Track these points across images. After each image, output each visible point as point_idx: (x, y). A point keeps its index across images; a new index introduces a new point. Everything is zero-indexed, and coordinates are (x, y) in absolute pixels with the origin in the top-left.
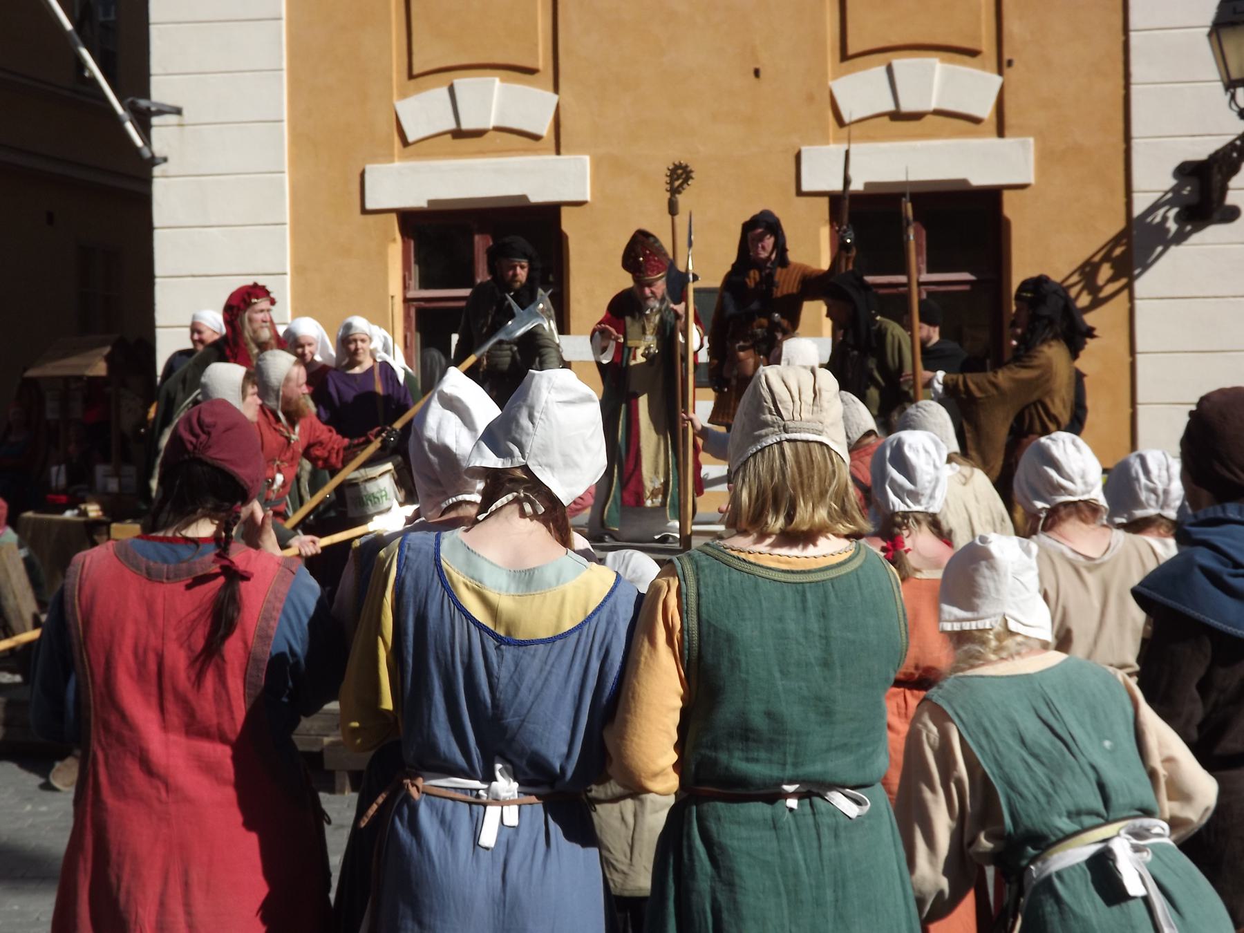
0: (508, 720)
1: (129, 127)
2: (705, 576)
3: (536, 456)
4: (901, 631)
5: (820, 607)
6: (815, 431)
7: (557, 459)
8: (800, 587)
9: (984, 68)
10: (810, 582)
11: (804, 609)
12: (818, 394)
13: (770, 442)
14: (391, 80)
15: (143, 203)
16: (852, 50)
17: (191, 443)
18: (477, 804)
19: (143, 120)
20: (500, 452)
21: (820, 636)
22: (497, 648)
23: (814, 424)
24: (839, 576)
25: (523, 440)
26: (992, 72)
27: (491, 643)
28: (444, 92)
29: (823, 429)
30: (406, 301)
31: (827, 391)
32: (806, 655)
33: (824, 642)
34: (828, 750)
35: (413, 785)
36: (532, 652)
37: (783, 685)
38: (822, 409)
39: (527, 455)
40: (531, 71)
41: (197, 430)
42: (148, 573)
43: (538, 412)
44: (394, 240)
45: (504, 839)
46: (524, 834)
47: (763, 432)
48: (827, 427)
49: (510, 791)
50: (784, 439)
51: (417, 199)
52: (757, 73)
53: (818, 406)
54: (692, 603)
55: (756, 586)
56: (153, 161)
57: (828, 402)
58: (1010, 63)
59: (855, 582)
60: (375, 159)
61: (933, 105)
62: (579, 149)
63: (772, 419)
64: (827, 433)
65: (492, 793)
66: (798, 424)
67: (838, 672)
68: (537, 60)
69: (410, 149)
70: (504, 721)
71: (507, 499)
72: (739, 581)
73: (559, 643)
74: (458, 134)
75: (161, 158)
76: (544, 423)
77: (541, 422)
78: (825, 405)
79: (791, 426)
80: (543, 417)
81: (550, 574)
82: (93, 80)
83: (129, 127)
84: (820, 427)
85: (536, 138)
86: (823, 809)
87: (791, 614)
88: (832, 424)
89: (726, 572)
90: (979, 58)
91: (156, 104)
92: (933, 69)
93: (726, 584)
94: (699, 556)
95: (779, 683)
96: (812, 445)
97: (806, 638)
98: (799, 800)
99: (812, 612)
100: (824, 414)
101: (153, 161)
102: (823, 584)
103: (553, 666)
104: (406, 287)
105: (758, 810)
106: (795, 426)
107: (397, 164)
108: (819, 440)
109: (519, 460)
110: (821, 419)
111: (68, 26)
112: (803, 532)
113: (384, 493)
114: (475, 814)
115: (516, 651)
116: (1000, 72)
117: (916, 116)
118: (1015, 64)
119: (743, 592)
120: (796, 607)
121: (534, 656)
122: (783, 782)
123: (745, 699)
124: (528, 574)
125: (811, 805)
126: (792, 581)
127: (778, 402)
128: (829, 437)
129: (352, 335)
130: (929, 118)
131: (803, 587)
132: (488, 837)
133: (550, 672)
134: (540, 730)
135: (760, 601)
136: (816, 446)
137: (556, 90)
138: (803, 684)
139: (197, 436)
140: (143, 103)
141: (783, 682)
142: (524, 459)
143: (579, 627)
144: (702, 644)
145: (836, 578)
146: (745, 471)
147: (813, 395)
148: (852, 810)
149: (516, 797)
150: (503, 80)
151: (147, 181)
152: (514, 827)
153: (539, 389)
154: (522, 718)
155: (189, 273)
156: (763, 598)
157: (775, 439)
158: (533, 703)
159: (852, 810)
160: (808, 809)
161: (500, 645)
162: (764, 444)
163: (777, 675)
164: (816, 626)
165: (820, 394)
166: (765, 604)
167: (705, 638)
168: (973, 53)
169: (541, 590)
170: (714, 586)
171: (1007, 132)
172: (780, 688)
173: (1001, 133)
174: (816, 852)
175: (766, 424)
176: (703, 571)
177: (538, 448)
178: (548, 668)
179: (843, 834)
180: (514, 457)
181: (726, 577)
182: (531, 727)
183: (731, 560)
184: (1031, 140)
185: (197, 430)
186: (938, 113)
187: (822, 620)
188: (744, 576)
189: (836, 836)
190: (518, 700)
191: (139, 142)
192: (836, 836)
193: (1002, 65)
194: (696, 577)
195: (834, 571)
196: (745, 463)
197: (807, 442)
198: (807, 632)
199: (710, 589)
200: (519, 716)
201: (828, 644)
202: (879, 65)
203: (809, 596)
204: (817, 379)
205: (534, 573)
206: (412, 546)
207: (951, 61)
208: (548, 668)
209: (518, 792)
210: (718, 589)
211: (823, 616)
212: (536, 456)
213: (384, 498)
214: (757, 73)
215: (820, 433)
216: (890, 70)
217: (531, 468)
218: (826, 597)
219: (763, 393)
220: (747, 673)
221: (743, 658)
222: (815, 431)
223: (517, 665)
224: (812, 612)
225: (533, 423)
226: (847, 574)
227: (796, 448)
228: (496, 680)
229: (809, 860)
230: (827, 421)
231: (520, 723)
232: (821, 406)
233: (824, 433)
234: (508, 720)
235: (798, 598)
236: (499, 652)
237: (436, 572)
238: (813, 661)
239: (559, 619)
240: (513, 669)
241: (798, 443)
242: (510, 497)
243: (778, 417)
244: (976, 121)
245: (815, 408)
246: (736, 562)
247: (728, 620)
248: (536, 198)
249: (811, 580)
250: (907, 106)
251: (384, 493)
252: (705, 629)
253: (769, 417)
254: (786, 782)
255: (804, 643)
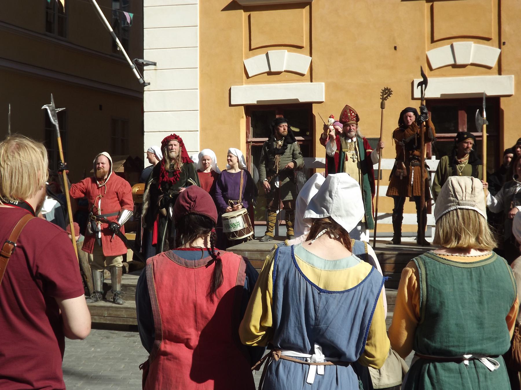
0: (321, 326)
1: (135, 70)
2: (429, 266)
3: (334, 212)
4: (514, 290)
5: (478, 278)
6: (472, 205)
7: (343, 213)
8: (469, 270)
9: (492, 46)
10: (474, 267)
11: (471, 279)
12: (474, 189)
13: (452, 209)
14: (242, 51)
15: (140, 101)
16: (435, 39)
17: (188, 207)
18: (305, 363)
19: (141, 68)
20: (317, 212)
21: (478, 290)
22: (319, 293)
23: (471, 202)
24: (486, 265)
25: (328, 206)
26: (496, 47)
27: (316, 292)
28: (264, 56)
29: (475, 205)
30: (247, 142)
31: (478, 188)
32: (472, 299)
33: (480, 293)
34: (482, 340)
35: (276, 354)
36: (334, 297)
37: (463, 312)
38: (475, 196)
39: (330, 212)
40: (301, 47)
41: (189, 201)
42: (186, 265)
43: (334, 193)
44: (243, 117)
45: (317, 381)
46: (326, 378)
47: (449, 204)
48: (477, 203)
49: (321, 359)
50: (458, 208)
51: (252, 100)
52: (395, 48)
53: (473, 194)
54: (424, 277)
55: (451, 270)
56: (144, 85)
57: (478, 193)
58: (504, 43)
59: (493, 267)
60: (235, 83)
61: (471, 62)
62: (320, 80)
63: (453, 199)
64: (477, 206)
65: (313, 359)
66: (464, 202)
67: (486, 306)
68: (303, 43)
69: (432, 72)
70: (320, 326)
71: (323, 232)
72: (444, 268)
73: (346, 293)
74: (270, 73)
75: (147, 83)
76: (337, 197)
77: (335, 197)
78: (477, 194)
79: (461, 203)
80: (336, 195)
81: (344, 263)
82: (121, 51)
83: (135, 70)
84: (474, 203)
85: (302, 75)
86: (480, 366)
87: (466, 281)
88: (479, 202)
89: (438, 264)
90: (491, 41)
91: (146, 61)
92: (471, 46)
93: (438, 270)
94: (425, 258)
95: (461, 311)
96: (470, 211)
97: (472, 291)
98: (469, 361)
99: (474, 280)
100: (476, 198)
101: (144, 85)
102: (479, 268)
103: (342, 304)
104: (247, 137)
105: (453, 365)
106: (463, 202)
107: (244, 86)
108: (473, 209)
109: (327, 215)
110: (475, 200)
111: (111, 30)
112: (464, 248)
113: (238, 224)
114: (304, 369)
115: (327, 295)
116: (500, 47)
117: (278, 73)
118: (506, 44)
119: (446, 273)
120: (468, 278)
121: (335, 298)
122: (464, 354)
123: (447, 319)
124: (334, 262)
125: (474, 364)
126: (466, 267)
127: (456, 192)
128: (478, 208)
129: (501, 202)
130: (468, 66)
131: (471, 270)
132: (311, 379)
133: (341, 306)
134: (335, 332)
135: (453, 276)
136: (472, 211)
137: (311, 55)
138: (471, 311)
139: (190, 204)
140: (141, 61)
141: (463, 311)
142: (329, 214)
143: (356, 287)
144: (428, 295)
145: (485, 265)
146: (441, 221)
147: (471, 190)
148: (492, 367)
149: (323, 362)
150: (288, 51)
151: (142, 92)
152: (322, 375)
153: (333, 183)
154: (328, 325)
155: (158, 131)
156: (454, 275)
157: (454, 208)
158: (333, 319)
159: (492, 367)
160: (473, 366)
161: (320, 292)
162: (450, 210)
163: (460, 307)
164: (476, 286)
165: (474, 189)
166: (455, 277)
167: (430, 292)
168: (488, 39)
169: (340, 269)
170: (433, 270)
171: (502, 73)
172: (462, 313)
173: (500, 73)
174: (477, 384)
175: (451, 202)
176: (428, 264)
177: (335, 209)
178: (340, 304)
179: (488, 377)
180: (324, 213)
181: (438, 267)
182: (331, 330)
183: (440, 259)
184: (513, 76)
185: (189, 201)
186: (472, 64)
187: (479, 283)
188: (446, 266)
189: (486, 377)
190: (326, 317)
191: (139, 77)
192: (486, 377)
193: (500, 45)
194: (425, 266)
195: (483, 262)
196: (441, 217)
197: (468, 209)
198: (472, 288)
199: (431, 272)
200: (326, 325)
201: (481, 294)
202: (448, 44)
203: (473, 273)
204: (474, 183)
205: (337, 262)
206: (281, 252)
207: (479, 43)
208: (340, 304)
209: (324, 360)
210: (435, 272)
211: (480, 282)
212: (334, 212)
213: (238, 226)
214: (395, 48)
215: (474, 206)
216: (452, 47)
217: (332, 217)
218: (481, 274)
219: (450, 188)
220: (448, 307)
221: (446, 301)
222: (472, 205)
223: (327, 302)
224: (474, 280)
225: (332, 198)
226: (489, 264)
227: (463, 213)
228: (318, 308)
229: (474, 388)
230: (477, 201)
231: (326, 327)
232: (475, 195)
233: (476, 206)
234: (321, 326)
235: (469, 275)
236: (320, 296)
237: (293, 261)
238: (475, 301)
239: (347, 281)
240: (325, 303)
241: (464, 210)
242: (324, 231)
243: (455, 199)
244: (489, 68)
245: (472, 195)
246: (442, 260)
247: (439, 285)
248: (302, 100)
249: (474, 266)
250: (459, 62)
251: (238, 224)
252: (429, 289)
253: (452, 198)
254: (466, 353)
255: (471, 294)
